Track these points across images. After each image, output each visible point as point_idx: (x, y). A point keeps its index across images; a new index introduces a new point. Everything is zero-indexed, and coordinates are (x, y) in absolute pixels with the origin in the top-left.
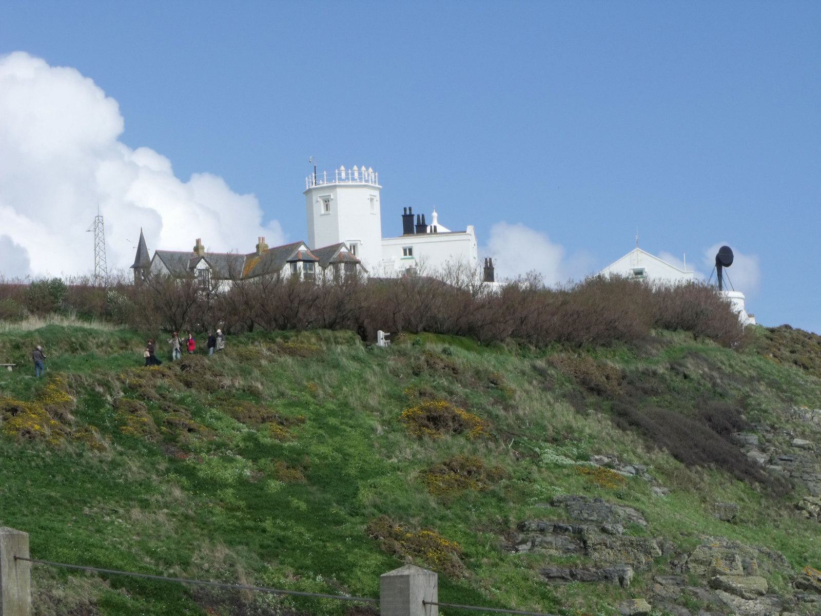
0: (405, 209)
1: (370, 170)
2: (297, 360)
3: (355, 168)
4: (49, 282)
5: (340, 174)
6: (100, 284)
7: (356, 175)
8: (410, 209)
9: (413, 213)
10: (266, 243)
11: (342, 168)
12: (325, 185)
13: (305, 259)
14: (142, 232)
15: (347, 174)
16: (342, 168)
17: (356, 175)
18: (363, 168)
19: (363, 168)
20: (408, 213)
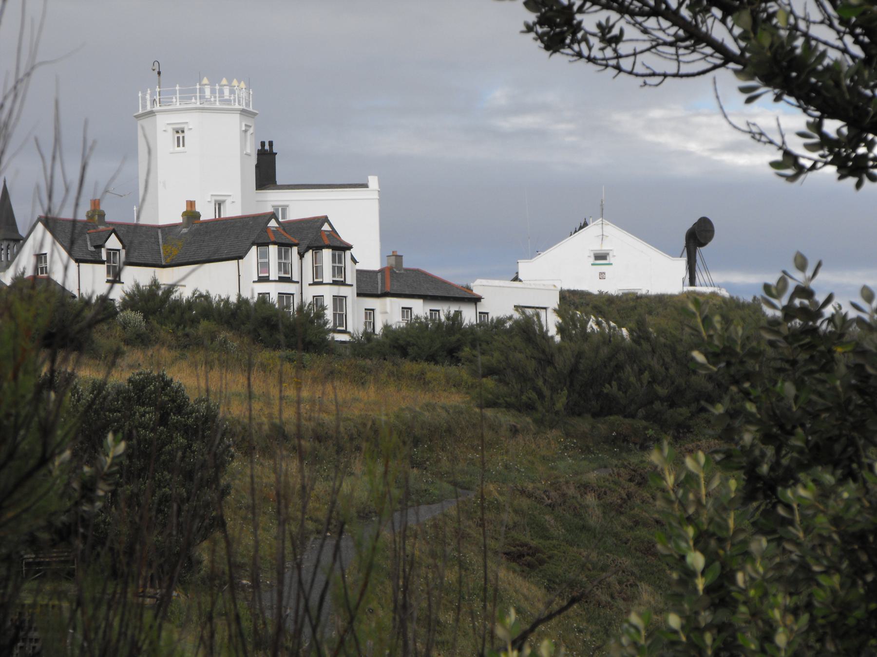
0: (263, 144)
1: (243, 85)
2: (264, 367)
3: (224, 82)
4: (94, 300)
5: (202, 91)
6: (744, 480)
7: (226, 91)
8: (271, 144)
9: (274, 151)
10: (197, 210)
11: (205, 81)
12: (178, 106)
13: (280, 241)
14: (5, 182)
15: (213, 92)
16: (205, 81)
17: (226, 91)
18: (235, 83)
19: (235, 83)
20: (267, 147)
